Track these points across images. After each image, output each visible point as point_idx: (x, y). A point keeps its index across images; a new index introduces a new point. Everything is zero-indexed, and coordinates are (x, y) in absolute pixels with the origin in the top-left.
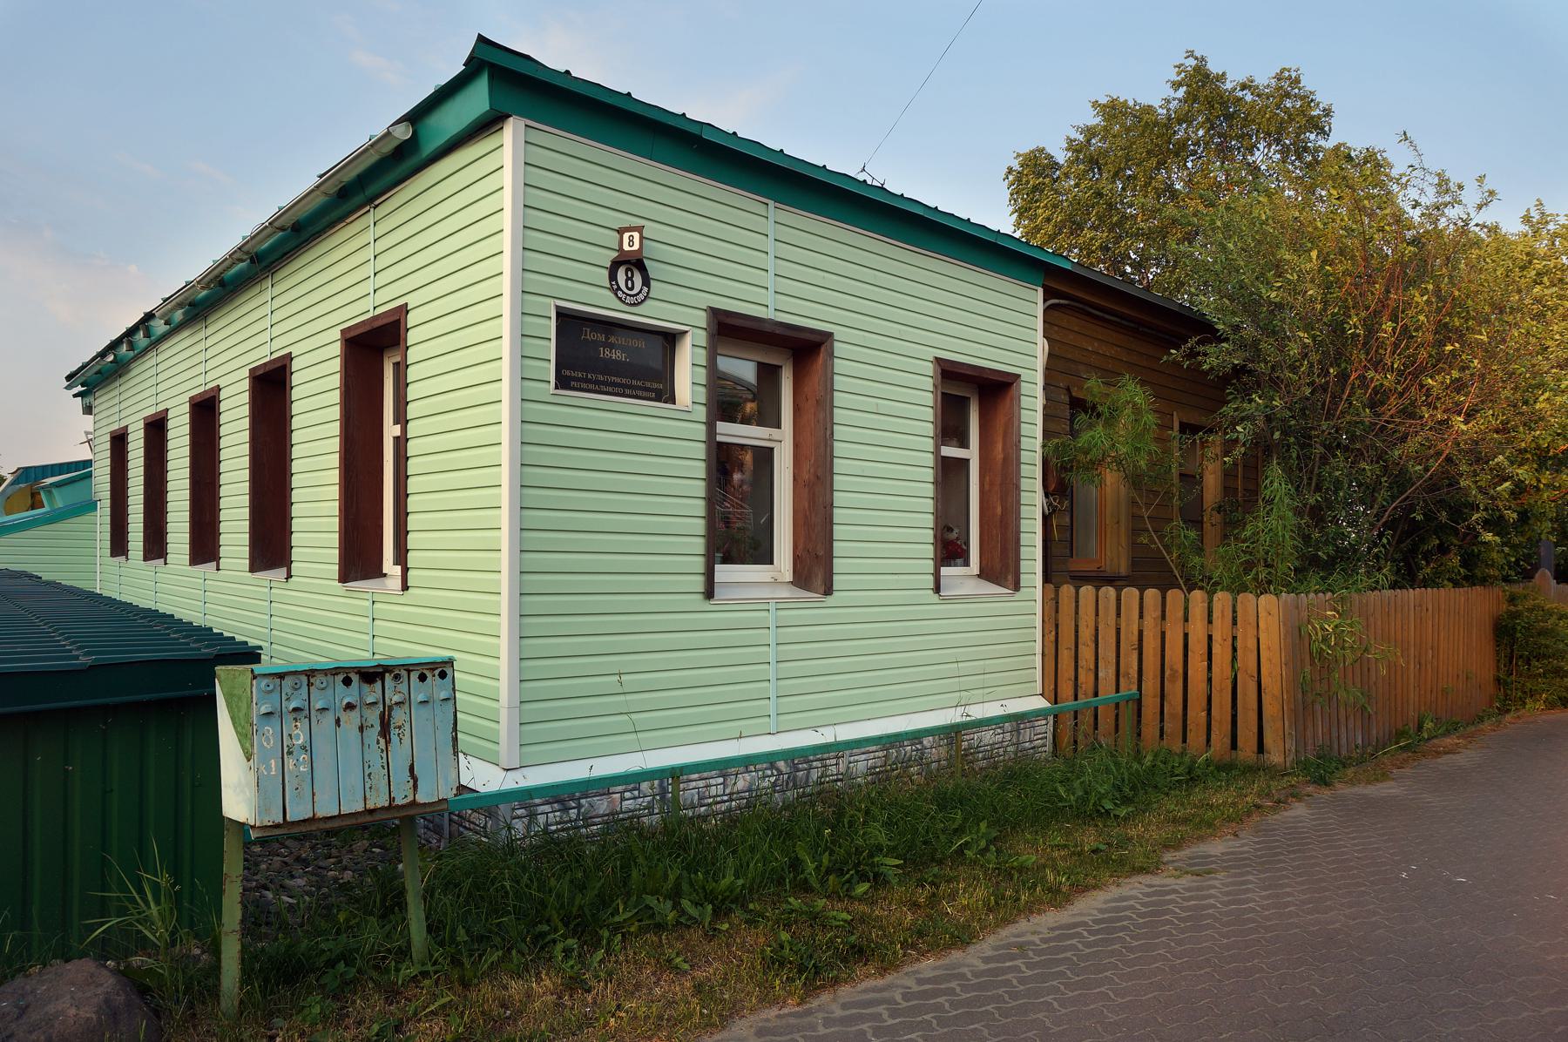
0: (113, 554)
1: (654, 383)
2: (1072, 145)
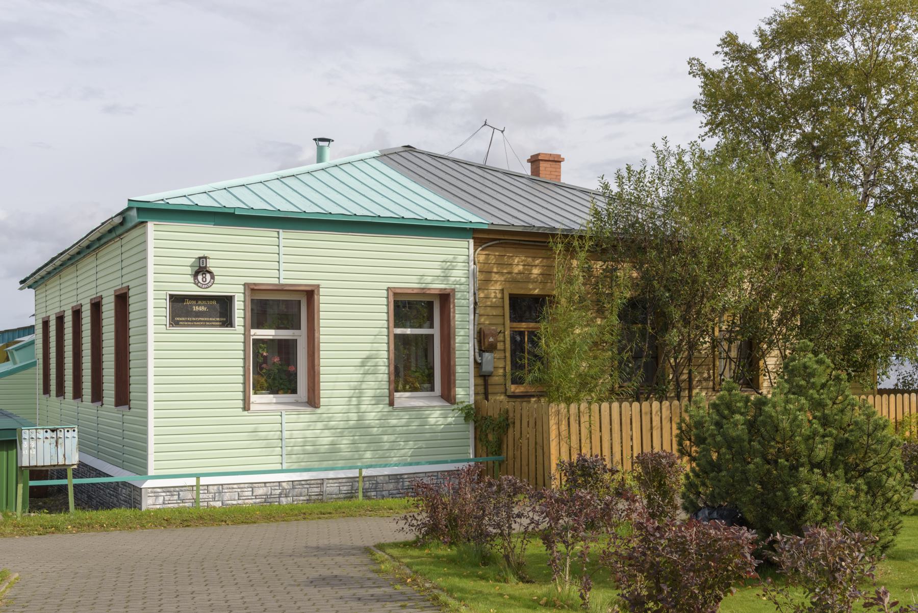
0: (93, 401)
1: (227, 321)
2: (762, 35)
